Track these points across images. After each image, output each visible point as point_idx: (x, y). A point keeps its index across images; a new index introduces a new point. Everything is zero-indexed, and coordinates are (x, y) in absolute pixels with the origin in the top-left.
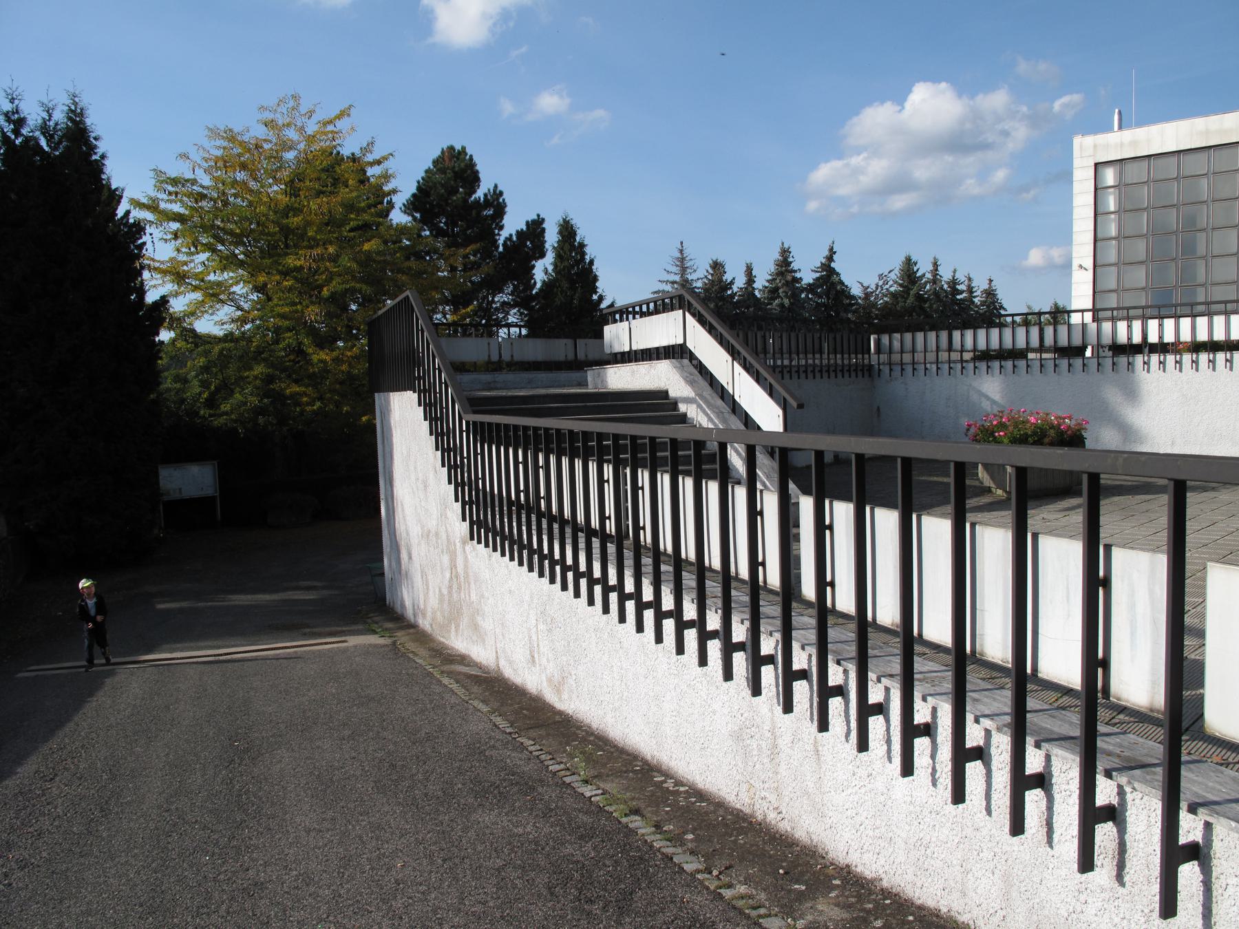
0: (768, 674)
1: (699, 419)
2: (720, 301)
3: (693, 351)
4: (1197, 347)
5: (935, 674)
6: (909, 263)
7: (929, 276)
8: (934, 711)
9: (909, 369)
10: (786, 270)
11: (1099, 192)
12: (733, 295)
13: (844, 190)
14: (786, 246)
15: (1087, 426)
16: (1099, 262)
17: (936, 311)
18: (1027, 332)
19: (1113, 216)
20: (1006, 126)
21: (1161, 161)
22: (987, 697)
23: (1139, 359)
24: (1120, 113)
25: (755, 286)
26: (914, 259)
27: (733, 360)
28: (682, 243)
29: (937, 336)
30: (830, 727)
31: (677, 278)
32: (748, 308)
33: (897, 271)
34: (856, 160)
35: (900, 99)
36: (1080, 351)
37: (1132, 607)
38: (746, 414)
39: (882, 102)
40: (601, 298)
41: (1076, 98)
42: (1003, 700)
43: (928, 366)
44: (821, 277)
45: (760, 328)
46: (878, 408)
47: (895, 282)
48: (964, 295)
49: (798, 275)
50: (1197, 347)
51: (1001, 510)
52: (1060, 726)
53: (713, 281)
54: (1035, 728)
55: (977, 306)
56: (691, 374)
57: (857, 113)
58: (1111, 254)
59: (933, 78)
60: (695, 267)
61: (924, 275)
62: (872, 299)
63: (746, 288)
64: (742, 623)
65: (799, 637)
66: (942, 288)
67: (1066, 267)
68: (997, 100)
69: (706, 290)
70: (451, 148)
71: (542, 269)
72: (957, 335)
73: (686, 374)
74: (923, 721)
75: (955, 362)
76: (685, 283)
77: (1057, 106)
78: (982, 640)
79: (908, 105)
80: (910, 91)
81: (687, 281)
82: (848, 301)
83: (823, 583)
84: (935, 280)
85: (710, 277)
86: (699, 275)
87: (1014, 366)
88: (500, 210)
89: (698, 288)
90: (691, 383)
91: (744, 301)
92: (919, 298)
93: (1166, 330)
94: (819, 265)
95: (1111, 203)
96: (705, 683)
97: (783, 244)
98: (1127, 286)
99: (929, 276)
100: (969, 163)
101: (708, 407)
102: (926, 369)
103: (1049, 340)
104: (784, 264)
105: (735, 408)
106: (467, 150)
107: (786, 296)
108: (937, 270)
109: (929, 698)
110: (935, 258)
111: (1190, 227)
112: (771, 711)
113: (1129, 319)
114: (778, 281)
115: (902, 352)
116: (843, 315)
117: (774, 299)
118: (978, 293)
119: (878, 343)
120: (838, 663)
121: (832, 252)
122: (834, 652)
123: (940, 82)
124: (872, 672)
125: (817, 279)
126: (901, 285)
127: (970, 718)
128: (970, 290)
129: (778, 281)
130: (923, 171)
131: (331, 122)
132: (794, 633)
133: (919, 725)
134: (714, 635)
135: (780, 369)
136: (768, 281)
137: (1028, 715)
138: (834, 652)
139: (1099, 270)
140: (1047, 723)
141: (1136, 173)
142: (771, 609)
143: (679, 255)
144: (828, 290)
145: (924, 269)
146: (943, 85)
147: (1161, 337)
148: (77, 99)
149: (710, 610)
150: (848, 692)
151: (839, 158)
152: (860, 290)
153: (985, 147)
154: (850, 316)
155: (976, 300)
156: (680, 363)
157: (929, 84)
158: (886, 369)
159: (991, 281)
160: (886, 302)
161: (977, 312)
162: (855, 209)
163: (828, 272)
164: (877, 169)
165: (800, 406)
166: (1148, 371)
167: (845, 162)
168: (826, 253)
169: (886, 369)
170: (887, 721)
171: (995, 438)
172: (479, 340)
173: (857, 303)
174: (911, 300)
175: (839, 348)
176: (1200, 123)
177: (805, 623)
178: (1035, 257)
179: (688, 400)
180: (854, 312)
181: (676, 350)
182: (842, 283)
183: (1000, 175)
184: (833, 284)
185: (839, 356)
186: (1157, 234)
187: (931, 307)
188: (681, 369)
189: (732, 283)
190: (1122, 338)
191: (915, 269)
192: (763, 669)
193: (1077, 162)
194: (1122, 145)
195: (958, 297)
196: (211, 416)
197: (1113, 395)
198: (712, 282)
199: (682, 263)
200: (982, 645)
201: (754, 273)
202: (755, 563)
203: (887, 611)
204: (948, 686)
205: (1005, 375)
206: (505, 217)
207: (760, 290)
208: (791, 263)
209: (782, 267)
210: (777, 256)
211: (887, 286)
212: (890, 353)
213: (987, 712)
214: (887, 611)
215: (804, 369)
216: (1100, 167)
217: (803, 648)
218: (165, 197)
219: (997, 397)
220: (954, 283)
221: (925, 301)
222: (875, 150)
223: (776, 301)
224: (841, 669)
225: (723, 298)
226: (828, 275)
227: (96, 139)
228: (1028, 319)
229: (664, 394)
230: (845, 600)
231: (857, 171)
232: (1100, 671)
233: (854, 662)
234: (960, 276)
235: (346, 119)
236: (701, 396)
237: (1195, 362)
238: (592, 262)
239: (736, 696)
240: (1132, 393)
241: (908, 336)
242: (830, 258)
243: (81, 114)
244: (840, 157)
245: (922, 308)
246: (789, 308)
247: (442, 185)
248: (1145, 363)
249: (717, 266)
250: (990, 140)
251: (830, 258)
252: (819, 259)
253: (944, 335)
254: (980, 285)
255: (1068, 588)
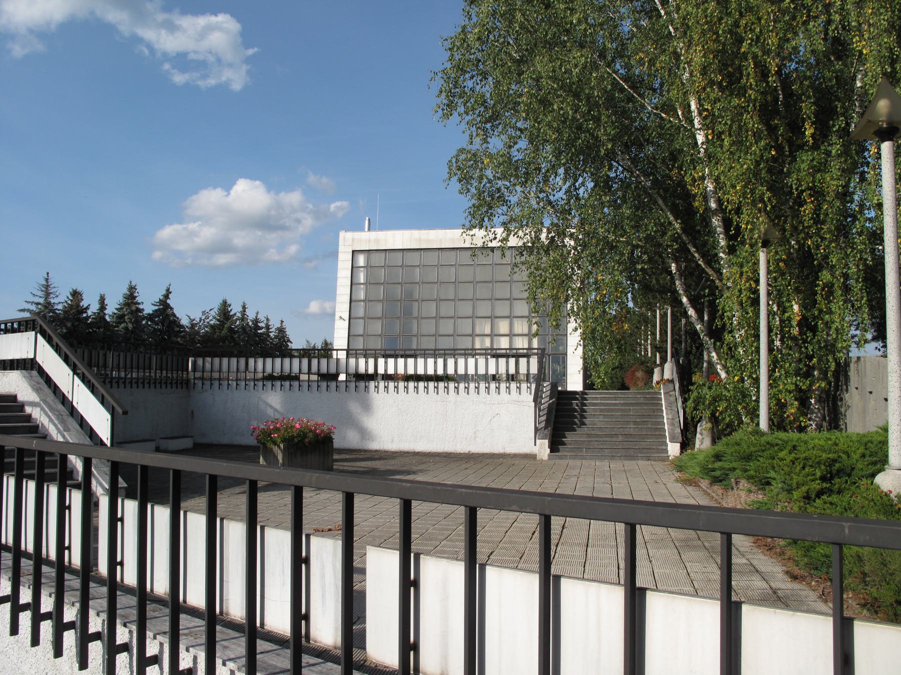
0: (70, 638)
1: (42, 419)
2: (76, 321)
3: (41, 364)
4: (407, 378)
5: (198, 629)
6: (225, 305)
7: (239, 315)
8: (195, 658)
9: (216, 383)
10: (132, 302)
11: (354, 270)
12: (88, 318)
13: (183, 246)
14: (133, 284)
15: (335, 431)
16: (352, 316)
17: (243, 340)
18: (300, 362)
19: (362, 286)
20: (299, 215)
21: (393, 254)
22: (234, 644)
23: (372, 384)
24: (369, 220)
25: (106, 312)
27: (74, 374)
28: (48, 273)
29: (238, 362)
31: (42, 301)
32: (99, 328)
33: (216, 310)
34: (193, 226)
35: (228, 188)
36: (336, 376)
37: (323, 577)
38: (82, 417)
39: (215, 188)
41: (345, 204)
42: (240, 647)
43: (230, 382)
45: (103, 348)
46: (192, 412)
47: (215, 318)
48: (263, 330)
49: (141, 307)
50: (407, 378)
51: (274, 490)
52: (283, 661)
53: (72, 305)
54: (265, 665)
55: (272, 339)
56: (38, 383)
57: (196, 193)
58: (360, 312)
59: (251, 177)
60: (57, 294)
61: (235, 314)
62: (196, 328)
63: (98, 313)
64: (50, 596)
65: (96, 605)
66: (248, 324)
67: (331, 316)
68: (294, 198)
69: (65, 311)
72: (251, 361)
73: (33, 383)
74: (187, 667)
75: (249, 380)
76: (48, 305)
77: (333, 207)
78: (227, 603)
79: (233, 192)
80: (234, 183)
81: (49, 303)
82: (178, 329)
83: (114, 563)
84: (243, 318)
85: (69, 302)
86: (61, 300)
87: (291, 385)
89: (59, 310)
90: (37, 390)
91: (96, 323)
92: (231, 330)
93: (390, 366)
94: (158, 300)
95: (362, 278)
96: (16, 648)
97: (131, 282)
98: (370, 333)
99: (239, 315)
100: (273, 238)
101: (50, 411)
102: (229, 384)
103: (314, 368)
104: (131, 297)
105: (73, 411)
107: (131, 322)
108: (245, 311)
109: (191, 649)
110: (244, 303)
111: (409, 298)
112: (71, 668)
113: (366, 356)
114: (125, 310)
115: (212, 371)
116: (174, 339)
117: (121, 323)
118: (273, 330)
119: (194, 364)
120: (125, 625)
121: (168, 292)
122: (123, 616)
123: (256, 180)
124: (150, 631)
125: (156, 311)
126: (218, 320)
127: (219, 662)
128: (268, 327)
129: (125, 310)
130: (241, 239)
132: (91, 603)
133: (183, 671)
134: (25, 607)
135: (116, 380)
136: (117, 309)
137: (258, 657)
138: (123, 616)
139: (352, 321)
140: (273, 660)
141: (378, 260)
142: (73, 582)
143: (45, 283)
144: (164, 319)
145: (235, 309)
146: (258, 183)
147: (386, 370)
149: (24, 586)
150: (132, 648)
151: (181, 223)
152: (188, 321)
153: (283, 228)
154: (179, 339)
155: (271, 334)
156: (29, 373)
157: (248, 181)
158: (199, 383)
159: (282, 322)
160: (207, 332)
161: (271, 343)
162: (189, 261)
163: (164, 307)
164: (207, 234)
165: (125, 413)
166: (378, 393)
167: (185, 226)
168: (164, 292)
169: (199, 383)
170: (161, 669)
171: (272, 438)
173: (185, 331)
174: (225, 331)
175: (164, 367)
176: (416, 233)
177: (99, 592)
178: (314, 307)
179: (33, 404)
180: (182, 337)
181: (27, 362)
182: (174, 315)
183: (293, 249)
184: (168, 316)
185: (164, 372)
186: (389, 300)
187: (239, 337)
188: (30, 379)
189: (87, 308)
190: (362, 370)
191: (229, 309)
192: (66, 634)
193: (341, 249)
194: (370, 241)
195: (259, 331)
197: (354, 407)
198: (71, 306)
199: (47, 289)
200: (227, 607)
201: (106, 302)
202: (62, 547)
203: (160, 585)
204: (203, 639)
205: (284, 391)
207: (110, 316)
208: (136, 297)
209: (128, 299)
210: (126, 291)
211: (208, 320)
212: (203, 372)
213: (232, 656)
214: (160, 585)
215: (136, 380)
216: (355, 252)
217: (98, 615)
219: (278, 407)
220: (256, 321)
221: (235, 333)
222: (206, 220)
223: (122, 325)
224: (127, 630)
225: (79, 320)
226: (164, 308)
228: (307, 353)
229: (14, 398)
230: (130, 577)
231: (193, 234)
232: (303, 622)
233: (135, 623)
234: (261, 317)
236: (45, 401)
237: (406, 388)
239: (42, 658)
240: (367, 407)
241: (217, 360)
242: (167, 296)
244: (180, 222)
245: (232, 338)
248: (375, 387)
249: (76, 294)
250: (288, 224)
251: (167, 296)
252: (158, 296)
253: (242, 361)
254: (275, 324)
255: (283, 565)
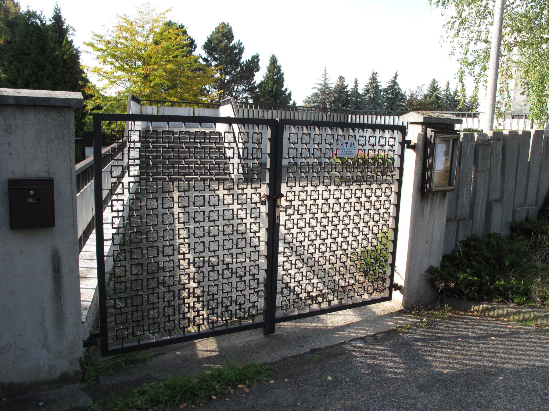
12: (348, 91)
26: (436, 80)
29: (372, 117)
30: (56, 224)
40: (286, 89)
44: (390, 86)
66: (450, 94)
70: (223, 23)
71: (259, 77)
81: (326, 84)
88: (241, 51)
92: (437, 97)
106: (229, 24)
108: (448, 85)
125: (389, 86)
131: (163, 13)
136: (365, 86)
148: (58, 4)
163: (394, 83)
168: (394, 75)
172: (185, 108)
184: (396, 89)
196: (107, 129)
206: (243, 53)
210: (370, 76)
218: (96, 42)
227: (65, 20)
235: (169, 12)
238: (283, 74)
242: (395, 78)
243: (59, 10)
245: (437, 102)
246: (373, 98)
247: (217, 39)
251: (395, 78)
